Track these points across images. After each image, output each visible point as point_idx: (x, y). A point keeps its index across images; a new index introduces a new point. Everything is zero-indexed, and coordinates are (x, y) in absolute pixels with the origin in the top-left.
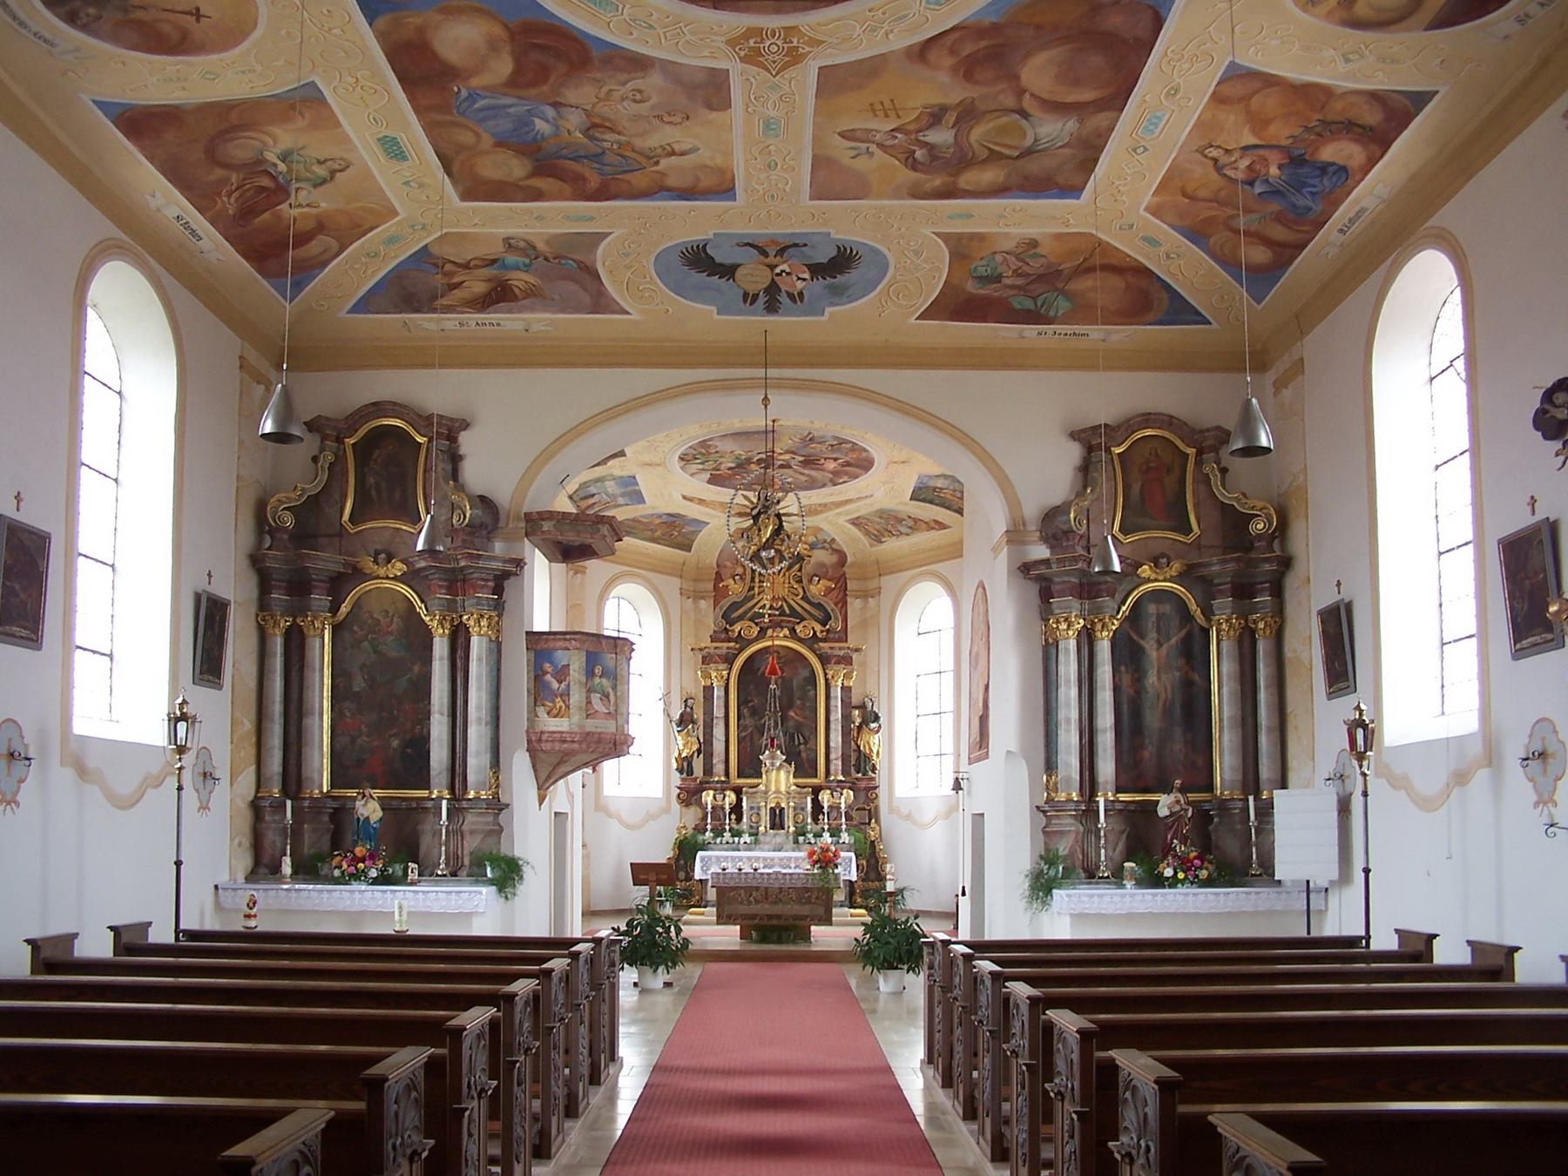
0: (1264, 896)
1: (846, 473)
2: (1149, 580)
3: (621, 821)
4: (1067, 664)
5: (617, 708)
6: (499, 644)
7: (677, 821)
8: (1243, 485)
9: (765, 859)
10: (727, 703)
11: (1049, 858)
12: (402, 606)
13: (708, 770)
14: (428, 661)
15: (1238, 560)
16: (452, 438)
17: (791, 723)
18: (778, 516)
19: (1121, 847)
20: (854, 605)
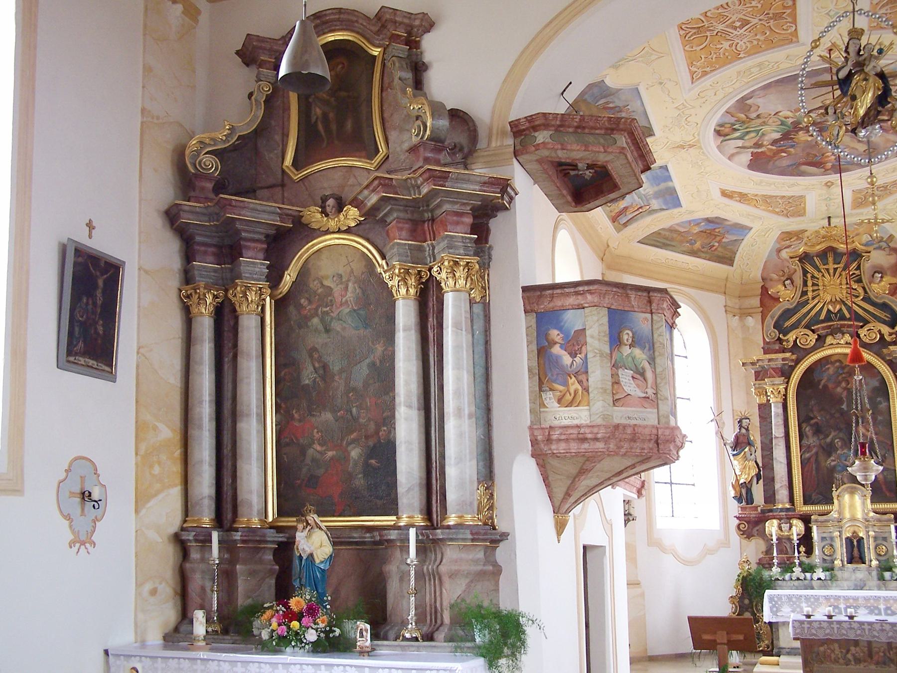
3: (676, 556)
5: (658, 394)
6: (486, 307)
7: (735, 556)
9: (846, 599)
10: (785, 423)
12: (358, 267)
13: (770, 497)
14: (389, 336)
16: (413, 43)
18: (881, 76)
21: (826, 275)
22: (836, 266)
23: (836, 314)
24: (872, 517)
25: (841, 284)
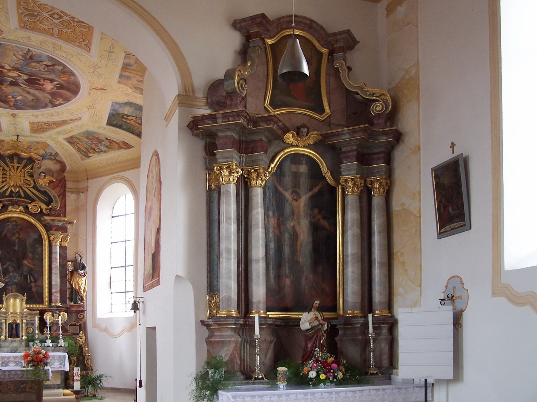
0: (388, 391)
1: (61, 96)
2: (292, 146)
4: (228, 204)
8: (364, 74)
11: (213, 363)
15: (364, 130)
17: (25, 269)
19: (270, 354)
20: (71, 198)
21: (12, 169)
22: (19, 165)
23: (16, 194)
24: (25, 312)
25: (20, 176)
